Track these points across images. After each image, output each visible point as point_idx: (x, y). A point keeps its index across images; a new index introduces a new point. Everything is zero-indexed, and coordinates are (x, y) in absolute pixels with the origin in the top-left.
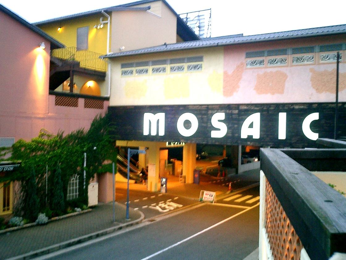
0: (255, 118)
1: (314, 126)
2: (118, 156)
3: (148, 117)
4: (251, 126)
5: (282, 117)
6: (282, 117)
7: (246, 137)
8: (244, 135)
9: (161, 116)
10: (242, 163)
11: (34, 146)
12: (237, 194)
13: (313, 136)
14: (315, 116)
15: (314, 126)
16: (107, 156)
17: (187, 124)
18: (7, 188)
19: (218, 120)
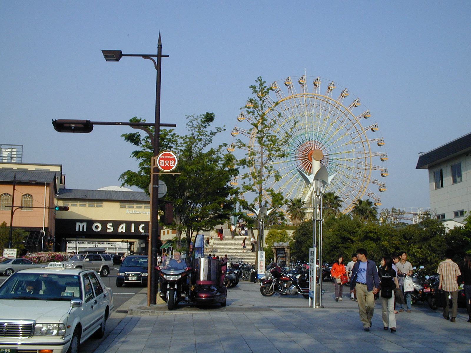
0: (124, 225)
1: (143, 228)
2: (202, 279)
3: (78, 224)
4: (122, 228)
5: (133, 226)
6: (133, 226)
7: (120, 231)
8: (120, 230)
9: (85, 224)
10: (68, 249)
11: (416, 246)
12: (76, 307)
13: (143, 231)
14: (143, 225)
15: (143, 228)
16: (295, 207)
17: (97, 227)
18: (10, 246)
19: (109, 225)
